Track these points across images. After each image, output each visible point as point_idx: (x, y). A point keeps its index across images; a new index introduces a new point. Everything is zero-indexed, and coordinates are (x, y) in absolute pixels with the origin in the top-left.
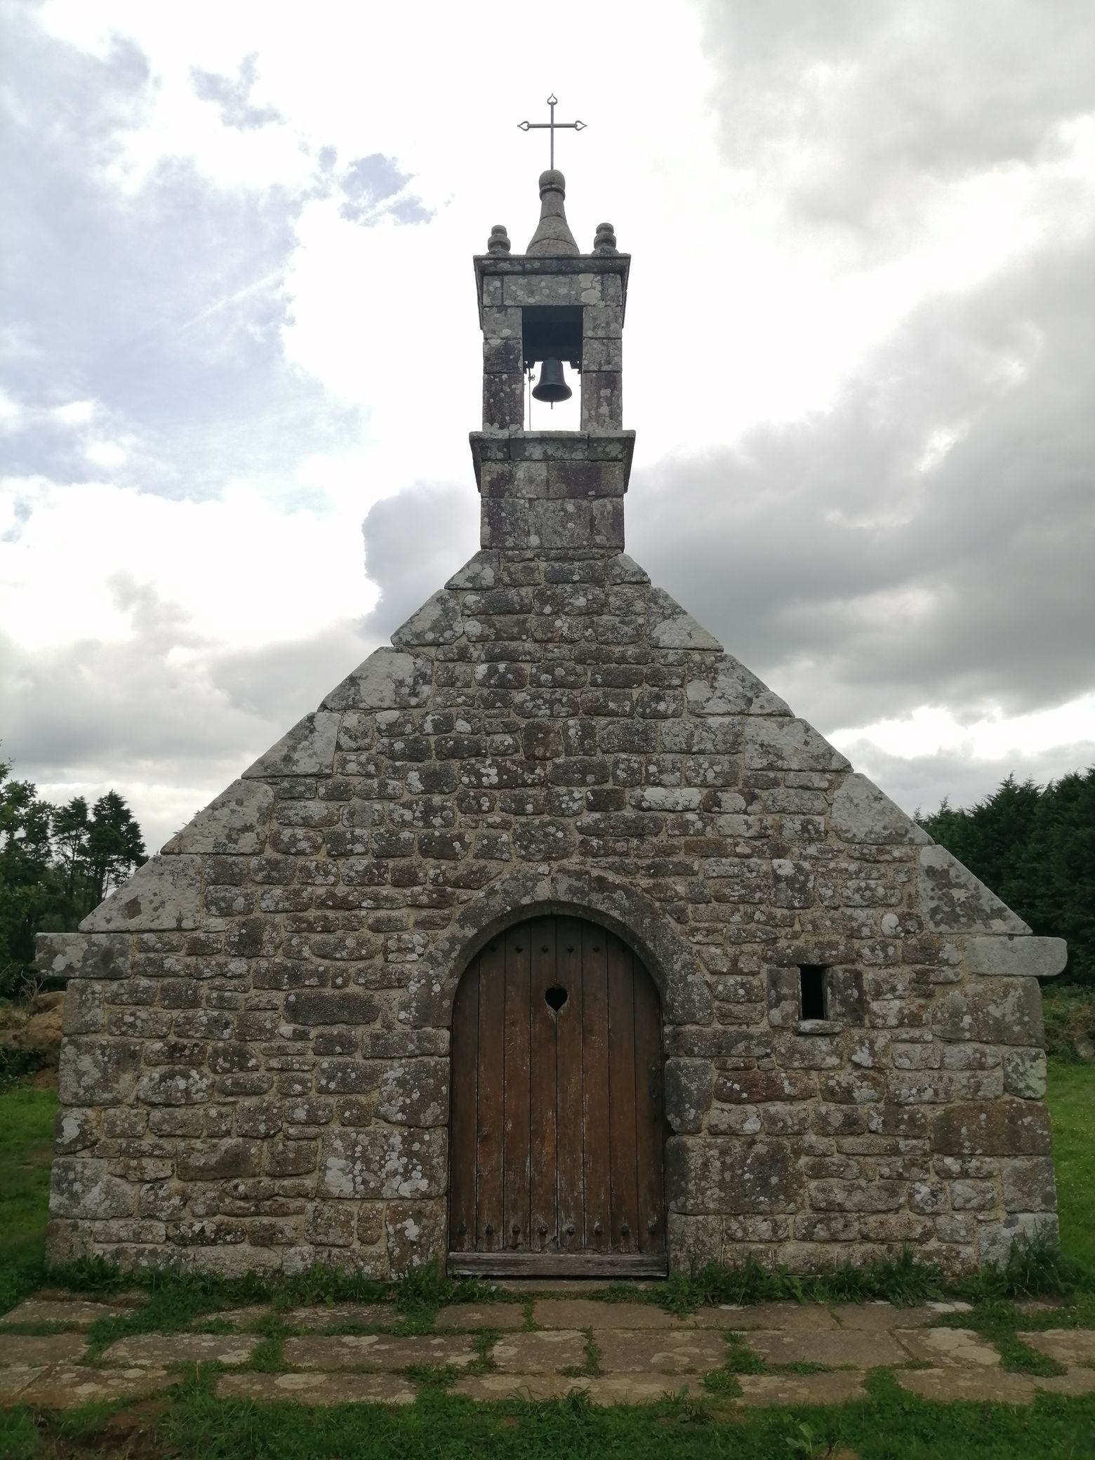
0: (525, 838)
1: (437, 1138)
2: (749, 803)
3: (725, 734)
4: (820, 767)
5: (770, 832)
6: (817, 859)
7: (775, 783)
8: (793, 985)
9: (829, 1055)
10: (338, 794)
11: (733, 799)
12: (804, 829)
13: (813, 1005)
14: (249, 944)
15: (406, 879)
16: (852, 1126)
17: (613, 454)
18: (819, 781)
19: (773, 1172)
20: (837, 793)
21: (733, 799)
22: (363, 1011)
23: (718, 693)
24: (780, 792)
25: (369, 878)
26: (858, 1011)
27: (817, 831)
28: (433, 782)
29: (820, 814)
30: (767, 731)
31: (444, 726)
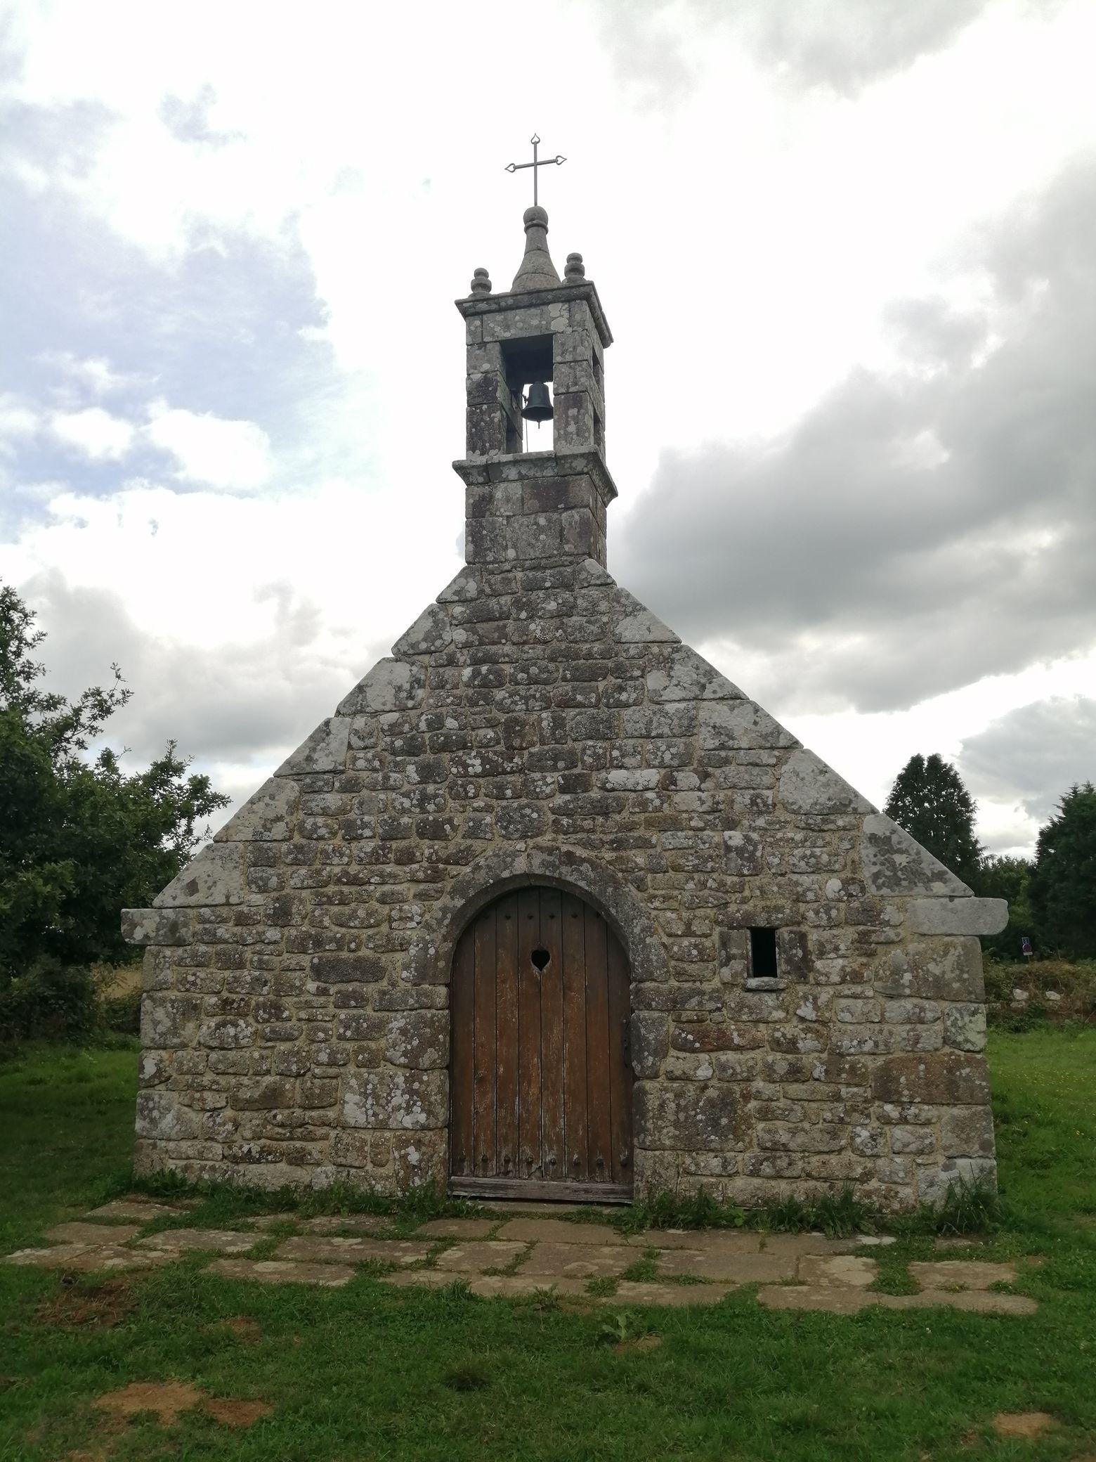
0: (505, 819)
1: (435, 1081)
2: (703, 781)
3: (680, 719)
4: (768, 745)
5: (721, 807)
6: (766, 830)
7: (727, 762)
8: (743, 946)
9: (778, 1009)
10: (351, 787)
11: (687, 778)
12: (753, 802)
13: (763, 963)
14: (281, 916)
15: (406, 858)
16: (796, 1074)
17: (579, 469)
18: (767, 758)
19: (723, 1114)
20: (785, 768)
21: (687, 778)
22: (373, 971)
23: (674, 682)
24: (730, 770)
25: (376, 858)
26: (803, 969)
27: (765, 804)
28: (427, 773)
29: (768, 788)
30: (719, 714)
31: (436, 724)
